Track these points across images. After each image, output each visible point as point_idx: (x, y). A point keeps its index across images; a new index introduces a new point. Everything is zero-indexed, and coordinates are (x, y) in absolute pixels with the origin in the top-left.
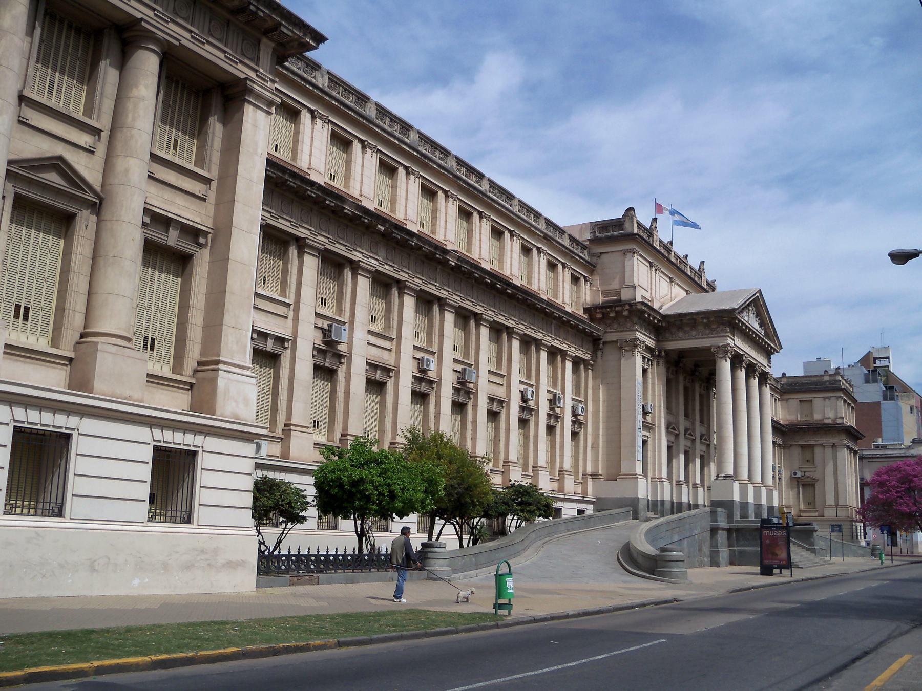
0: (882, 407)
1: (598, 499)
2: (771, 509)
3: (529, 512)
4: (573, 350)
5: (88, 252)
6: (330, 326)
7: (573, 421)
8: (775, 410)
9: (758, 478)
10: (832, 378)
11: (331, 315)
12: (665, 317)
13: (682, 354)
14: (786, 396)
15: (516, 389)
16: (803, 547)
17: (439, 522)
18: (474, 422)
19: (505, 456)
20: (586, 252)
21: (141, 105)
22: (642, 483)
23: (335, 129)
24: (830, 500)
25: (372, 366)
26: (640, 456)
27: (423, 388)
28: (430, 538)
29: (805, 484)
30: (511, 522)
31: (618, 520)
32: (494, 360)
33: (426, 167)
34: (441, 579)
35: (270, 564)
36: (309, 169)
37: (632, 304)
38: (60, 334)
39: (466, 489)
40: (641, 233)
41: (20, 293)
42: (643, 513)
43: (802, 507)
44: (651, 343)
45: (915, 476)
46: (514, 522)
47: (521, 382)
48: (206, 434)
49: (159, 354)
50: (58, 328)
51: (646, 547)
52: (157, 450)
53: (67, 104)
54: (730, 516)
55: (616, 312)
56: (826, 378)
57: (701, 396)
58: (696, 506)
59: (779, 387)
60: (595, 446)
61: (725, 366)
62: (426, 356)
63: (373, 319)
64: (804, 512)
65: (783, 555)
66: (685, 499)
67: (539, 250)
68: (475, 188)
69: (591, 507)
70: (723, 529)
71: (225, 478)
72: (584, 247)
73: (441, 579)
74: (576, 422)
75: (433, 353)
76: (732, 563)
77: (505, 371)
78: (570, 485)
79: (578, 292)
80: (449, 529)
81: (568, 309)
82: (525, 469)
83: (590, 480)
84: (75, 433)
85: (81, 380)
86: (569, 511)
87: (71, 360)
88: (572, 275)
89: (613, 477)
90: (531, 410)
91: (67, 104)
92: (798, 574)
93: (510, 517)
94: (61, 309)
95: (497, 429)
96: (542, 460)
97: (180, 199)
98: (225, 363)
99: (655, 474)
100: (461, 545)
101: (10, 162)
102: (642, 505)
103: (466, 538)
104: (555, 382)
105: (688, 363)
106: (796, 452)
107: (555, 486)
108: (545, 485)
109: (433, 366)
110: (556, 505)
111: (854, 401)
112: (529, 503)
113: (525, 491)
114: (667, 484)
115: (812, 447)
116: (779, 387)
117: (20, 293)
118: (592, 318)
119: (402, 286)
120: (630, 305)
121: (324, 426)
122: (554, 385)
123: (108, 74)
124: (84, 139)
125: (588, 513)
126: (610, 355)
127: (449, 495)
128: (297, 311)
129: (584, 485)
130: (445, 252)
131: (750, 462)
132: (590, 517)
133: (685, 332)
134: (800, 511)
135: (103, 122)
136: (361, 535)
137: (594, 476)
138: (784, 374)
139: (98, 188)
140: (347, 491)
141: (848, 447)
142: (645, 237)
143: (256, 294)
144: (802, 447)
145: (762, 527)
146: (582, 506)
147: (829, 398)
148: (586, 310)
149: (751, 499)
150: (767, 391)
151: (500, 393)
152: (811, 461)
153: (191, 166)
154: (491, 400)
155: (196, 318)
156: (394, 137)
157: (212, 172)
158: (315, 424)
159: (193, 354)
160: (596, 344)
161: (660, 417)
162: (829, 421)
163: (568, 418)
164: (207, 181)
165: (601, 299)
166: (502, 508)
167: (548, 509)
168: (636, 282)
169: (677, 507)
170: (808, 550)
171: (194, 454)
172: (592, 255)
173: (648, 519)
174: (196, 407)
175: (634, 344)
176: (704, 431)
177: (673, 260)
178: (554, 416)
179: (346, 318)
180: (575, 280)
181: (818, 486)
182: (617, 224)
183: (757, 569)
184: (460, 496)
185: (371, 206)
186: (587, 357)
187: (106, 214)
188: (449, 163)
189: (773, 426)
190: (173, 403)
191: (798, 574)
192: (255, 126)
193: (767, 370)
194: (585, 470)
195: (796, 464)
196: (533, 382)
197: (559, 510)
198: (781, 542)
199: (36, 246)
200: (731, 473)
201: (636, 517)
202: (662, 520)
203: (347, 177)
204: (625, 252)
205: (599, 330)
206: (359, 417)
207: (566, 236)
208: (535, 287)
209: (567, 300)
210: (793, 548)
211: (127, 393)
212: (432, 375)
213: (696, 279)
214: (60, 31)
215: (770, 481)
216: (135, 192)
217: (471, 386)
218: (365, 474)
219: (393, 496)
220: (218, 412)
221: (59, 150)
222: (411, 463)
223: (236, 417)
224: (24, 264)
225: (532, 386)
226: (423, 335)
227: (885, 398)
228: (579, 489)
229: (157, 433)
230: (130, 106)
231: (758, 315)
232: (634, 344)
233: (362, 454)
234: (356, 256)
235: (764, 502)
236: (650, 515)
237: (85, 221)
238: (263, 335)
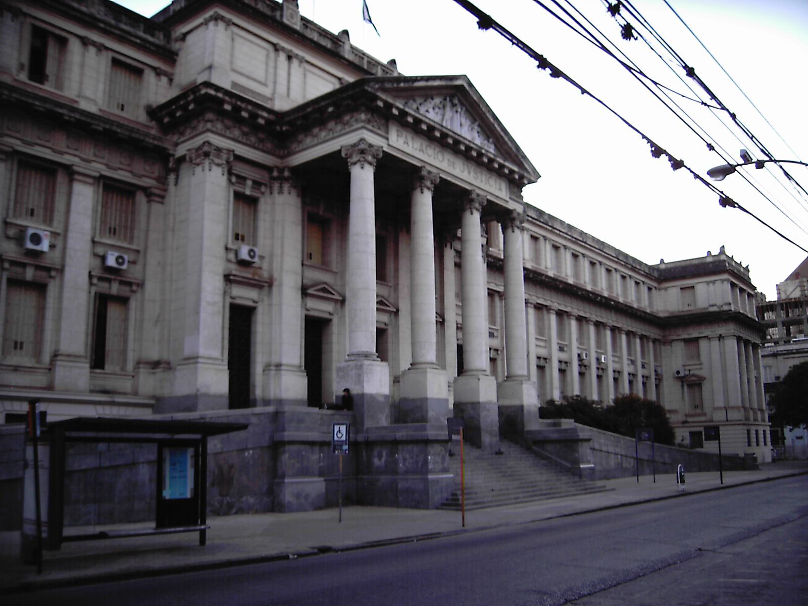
7: (579, 365)
12: (280, 116)
36: (79, 96)
67: (545, 238)
88: (532, 237)
115: (696, 340)
147: (714, 282)
181: (706, 386)
209: (549, 265)
225: (585, 350)
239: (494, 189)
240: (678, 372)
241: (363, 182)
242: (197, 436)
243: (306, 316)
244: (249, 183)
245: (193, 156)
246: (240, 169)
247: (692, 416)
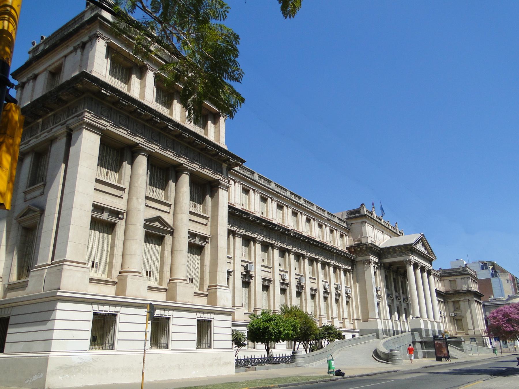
0: (492, 280)
1: (360, 330)
2: (440, 332)
3: (332, 337)
4: (343, 266)
5: (170, 249)
6: (247, 265)
8: (437, 285)
9: (432, 318)
11: (247, 260)
12: (382, 249)
13: (391, 264)
14: (443, 278)
15: (321, 284)
16: (458, 349)
17: (297, 343)
18: (306, 300)
19: (322, 313)
20: (345, 223)
21: (185, 194)
22: (379, 322)
24: (470, 327)
25: (264, 280)
26: (377, 310)
27: (284, 287)
28: (294, 349)
29: (457, 320)
30: (324, 342)
31: (370, 339)
32: (311, 273)
33: (278, 197)
34: (302, 367)
35: (240, 364)
37: (367, 245)
38: (162, 280)
39: (307, 328)
40: (368, 214)
41: (148, 267)
42: (381, 336)
44: (377, 260)
45: (511, 313)
46: (326, 342)
47: (323, 281)
48: (214, 313)
49: (195, 284)
50: (161, 278)
51: (383, 350)
52: (199, 321)
53: (159, 196)
54: (421, 335)
55: (360, 248)
56: (461, 269)
57: (402, 282)
58: (405, 331)
59: (439, 274)
60: (357, 307)
61: (411, 269)
62: (284, 274)
63: (263, 260)
64: (459, 333)
65: (445, 352)
66: (399, 329)
68: (298, 203)
69: (358, 334)
70: (418, 342)
71: (222, 329)
72: (344, 222)
73: (302, 367)
74: (348, 297)
75: (287, 272)
76: (424, 357)
77: (318, 277)
78: (348, 326)
79: (343, 241)
80: (301, 346)
81: (340, 249)
82: (328, 318)
83: (356, 322)
84: (171, 317)
85: (171, 297)
86: (348, 336)
87: (166, 290)
89: (366, 320)
90: (328, 293)
91: (159, 196)
92: (453, 361)
93: (324, 340)
94: (162, 271)
95: (315, 302)
96: (335, 314)
97: (199, 226)
98: (219, 286)
99: (383, 319)
100: (306, 353)
101: (145, 220)
102: (380, 332)
103: (308, 350)
104: (339, 280)
105: (394, 267)
106: (451, 305)
107: (341, 325)
108: (337, 325)
109: (287, 278)
110: (343, 334)
111: (476, 279)
112: (331, 333)
113: (330, 328)
114: (390, 322)
115: (458, 302)
116: (439, 274)
117: (148, 267)
118: (350, 252)
119: (273, 246)
120: (366, 245)
121: (247, 306)
122: (337, 281)
123: (172, 185)
124: (166, 208)
125: (357, 336)
126: (360, 267)
127: (301, 331)
128: (234, 260)
129: (354, 324)
130: (289, 230)
131: (430, 313)
132: (358, 338)
133: (391, 254)
134: (457, 333)
135: (171, 201)
136: (268, 351)
137: (358, 320)
138: (440, 268)
139: (172, 226)
140: (262, 332)
141: (476, 301)
142: (370, 215)
144: (453, 302)
145: (434, 339)
146: (354, 334)
148: (347, 248)
149: (430, 327)
150: (432, 278)
151: (315, 286)
152: (458, 309)
153: (201, 214)
154: (312, 290)
155: (207, 269)
156: (266, 187)
157: (208, 215)
158: (243, 305)
159: (207, 283)
160: (353, 263)
161: (383, 292)
162: (465, 289)
163: (344, 295)
164: (207, 218)
165: (353, 243)
166: (322, 336)
167: (340, 336)
168: (368, 235)
169: (396, 333)
170: (460, 350)
171: (211, 321)
172: (347, 225)
173: (384, 338)
174: (209, 303)
175: (369, 262)
176: (405, 297)
177: (383, 224)
178: (338, 295)
179: (252, 261)
180: (342, 236)
182: (358, 211)
183: (435, 359)
184: (306, 331)
185: (258, 215)
186: (350, 268)
187: (175, 235)
189: (436, 292)
190: (201, 302)
191: (453, 361)
192: (223, 196)
193: (431, 268)
194: (353, 318)
195: (452, 309)
196: (328, 281)
198: (444, 346)
199: (152, 249)
200: (419, 316)
201: (378, 337)
202: (390, 338)
203: (249, 204)
204: (362, 223)
205: (353, 257)
206: (261, 302)
207: (336, 218)
208: (325, 241)
209: (339, 245)
210: (449, 348)
211: (188, 300)
212: (287, 281)
213: (394, 231)
214: (155, 169)
215: (438, 318)
216: (185, 226)
217: (303, 284)
218: (268, 324)
219: (280, 332)
220: (218, 304)
221: (158, 214)
222: (285, 319)
223: (224, 305)
224: (148, 256)
225: (327, 282)
226: (282, 265)
227: (493, 276)
228: (352, 326)
229: (198, 315)
230: (181, 195)
232: (369, 262)
233: (268, 318)
234: (255, 236)
235: (436, 328)
236: (384, 336)
237: (168, 238)
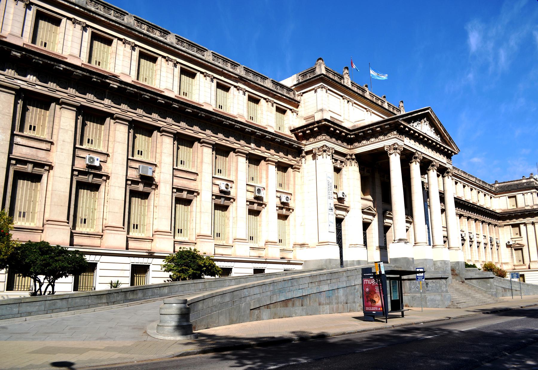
10: (528, 180)
23: (142, 50)
43: (516, 263)
110: (89, 258)
115: (518, 225)
118: (297, 136)
143: (213, 177)
188: (125, 19)
197: (227, 271)
231: (432, 124)
238: (180, 190)
239: (441, 159)
240: (509, 242)
241: (395, 162)
242: (398, 276)
243: (363, 222)
244: (339, 162)
245: (317, 152)
246: (336, 156)
247: (517, 266)
